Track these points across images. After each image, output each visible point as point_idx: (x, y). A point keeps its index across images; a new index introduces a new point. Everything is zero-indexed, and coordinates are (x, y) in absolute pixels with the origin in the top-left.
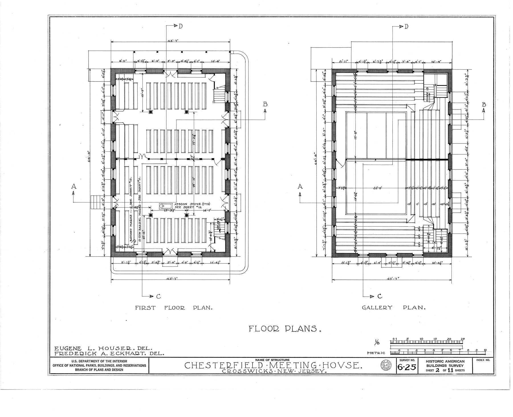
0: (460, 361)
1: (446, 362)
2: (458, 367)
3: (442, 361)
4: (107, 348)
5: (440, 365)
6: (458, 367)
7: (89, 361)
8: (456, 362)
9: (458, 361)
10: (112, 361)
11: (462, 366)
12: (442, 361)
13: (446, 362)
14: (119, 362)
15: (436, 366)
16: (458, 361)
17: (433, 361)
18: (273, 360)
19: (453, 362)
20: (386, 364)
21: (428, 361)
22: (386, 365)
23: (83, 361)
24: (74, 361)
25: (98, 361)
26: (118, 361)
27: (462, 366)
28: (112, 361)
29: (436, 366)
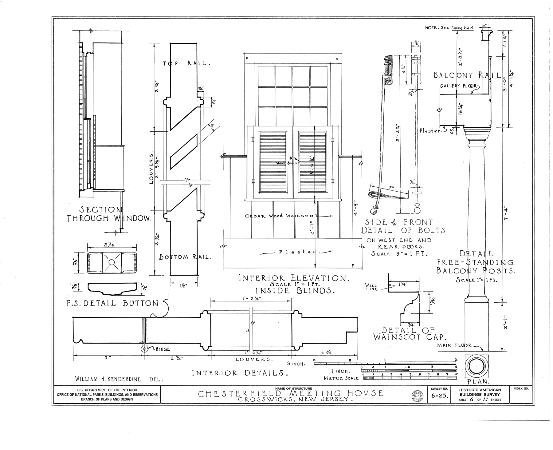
0: (496, 390)
2: (494, 396)
3: (477, 390)
4: (335, 278)
6: (494, 396)
7: (96, 390)
8: (492, 390)
9: (494, 390)
11: (499, 395)
12: (477, 390)
13: (419, 241)
14: (129, 390)
15: (471, 395)
16: (494, 390)
17: (466, 390)
19: (489, 390)
21: (462, 390)
24: (80, 390)
25: (105, 390)
26: (127, 390)
27: (499, 395)
29: (471, 395)
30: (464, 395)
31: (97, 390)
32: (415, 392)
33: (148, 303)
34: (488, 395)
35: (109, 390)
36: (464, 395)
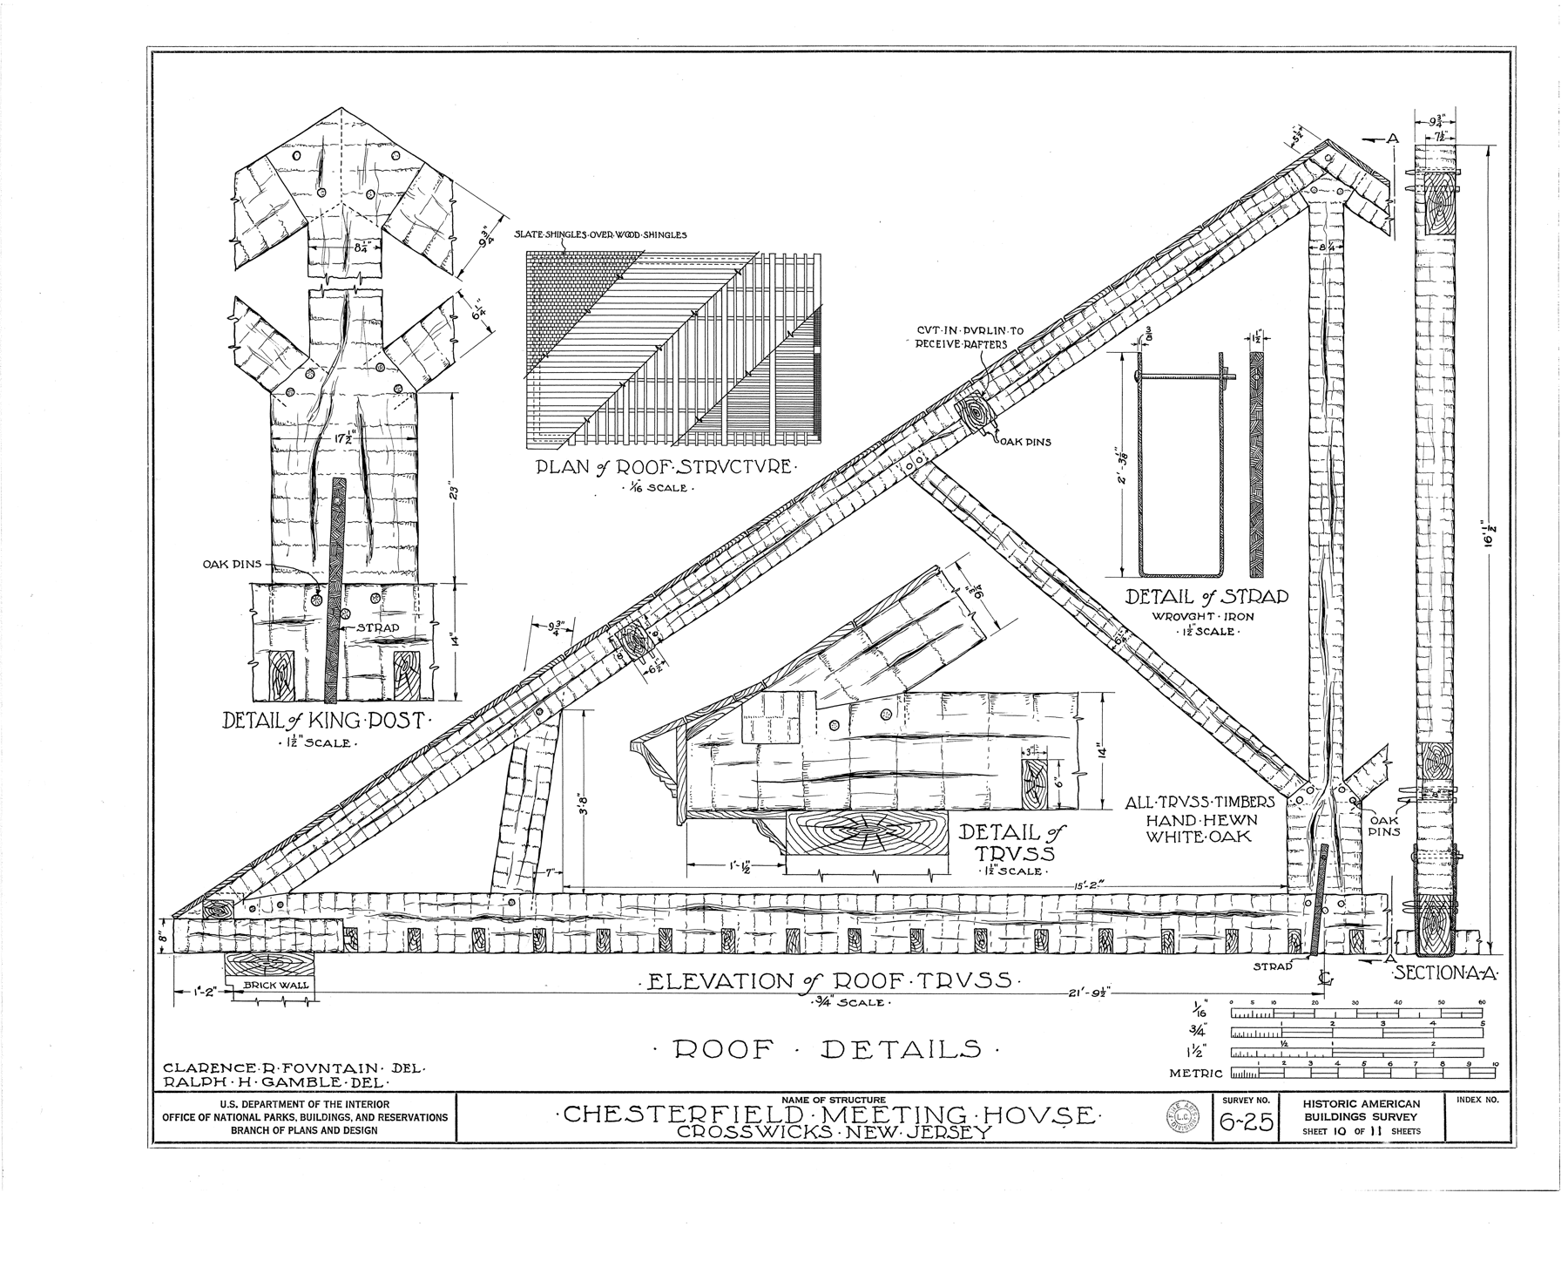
0: (1405, 1104)
1: (1365, 1107)
2: (1399, 1120)
3: (1353, 1104)
5: (1345, 1114)
6: (1399, 1120)
7: (273, 1105)
9: (1402, 1104)
10: (343, 1104)
12: (1353, 1104)
13: (1365, 1107)
14: (366, 1105)
15: (1335, 1117)
16: (1402, 1104)
17: (1323, 1104)
18: (1323, 1104)
19: (1386, 1104)
20: (1181, 1113)
22: (1181, 1116)
23: (257, 1103)
24: (228, 1104)
26: (360, 1104)
28: (343, 1104)
29: (1335, 1117)
30: (1316, 1118)
31: (278, 1104)
32: (1175, 1106)
33: (1333, 1104)
34: (1316, 1117)
35: (1357, 1131)
36: (1316, 1118)
